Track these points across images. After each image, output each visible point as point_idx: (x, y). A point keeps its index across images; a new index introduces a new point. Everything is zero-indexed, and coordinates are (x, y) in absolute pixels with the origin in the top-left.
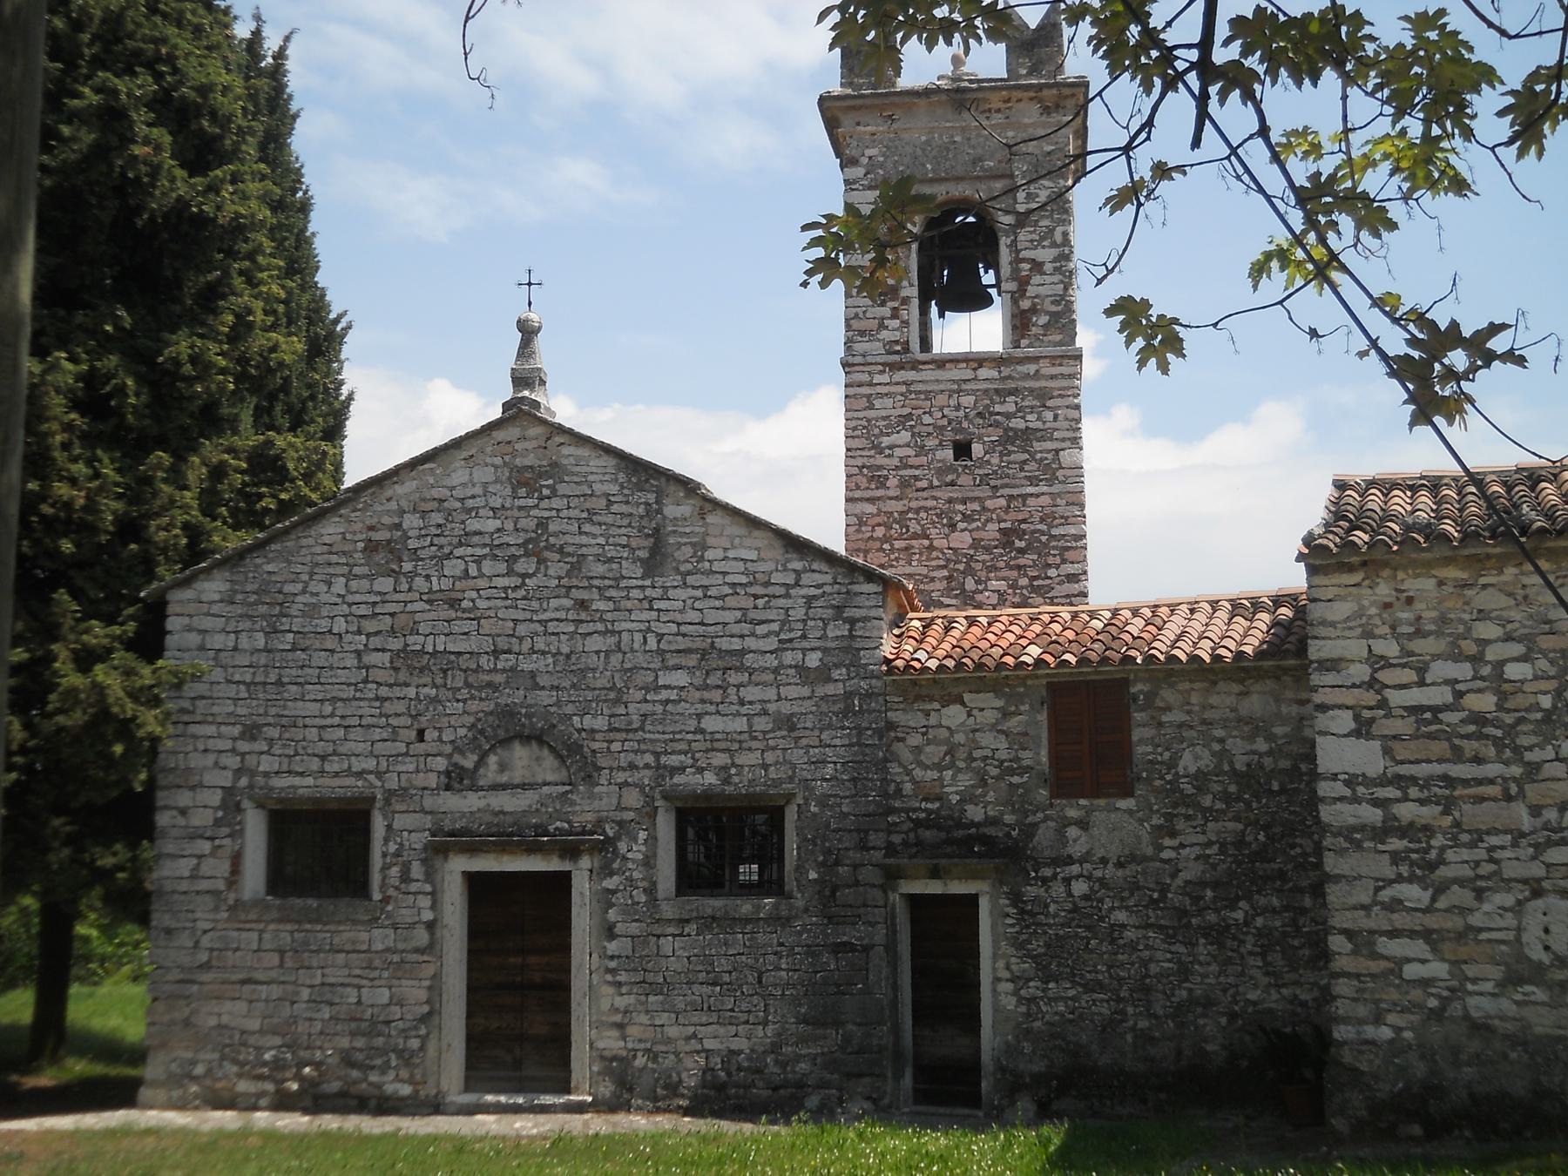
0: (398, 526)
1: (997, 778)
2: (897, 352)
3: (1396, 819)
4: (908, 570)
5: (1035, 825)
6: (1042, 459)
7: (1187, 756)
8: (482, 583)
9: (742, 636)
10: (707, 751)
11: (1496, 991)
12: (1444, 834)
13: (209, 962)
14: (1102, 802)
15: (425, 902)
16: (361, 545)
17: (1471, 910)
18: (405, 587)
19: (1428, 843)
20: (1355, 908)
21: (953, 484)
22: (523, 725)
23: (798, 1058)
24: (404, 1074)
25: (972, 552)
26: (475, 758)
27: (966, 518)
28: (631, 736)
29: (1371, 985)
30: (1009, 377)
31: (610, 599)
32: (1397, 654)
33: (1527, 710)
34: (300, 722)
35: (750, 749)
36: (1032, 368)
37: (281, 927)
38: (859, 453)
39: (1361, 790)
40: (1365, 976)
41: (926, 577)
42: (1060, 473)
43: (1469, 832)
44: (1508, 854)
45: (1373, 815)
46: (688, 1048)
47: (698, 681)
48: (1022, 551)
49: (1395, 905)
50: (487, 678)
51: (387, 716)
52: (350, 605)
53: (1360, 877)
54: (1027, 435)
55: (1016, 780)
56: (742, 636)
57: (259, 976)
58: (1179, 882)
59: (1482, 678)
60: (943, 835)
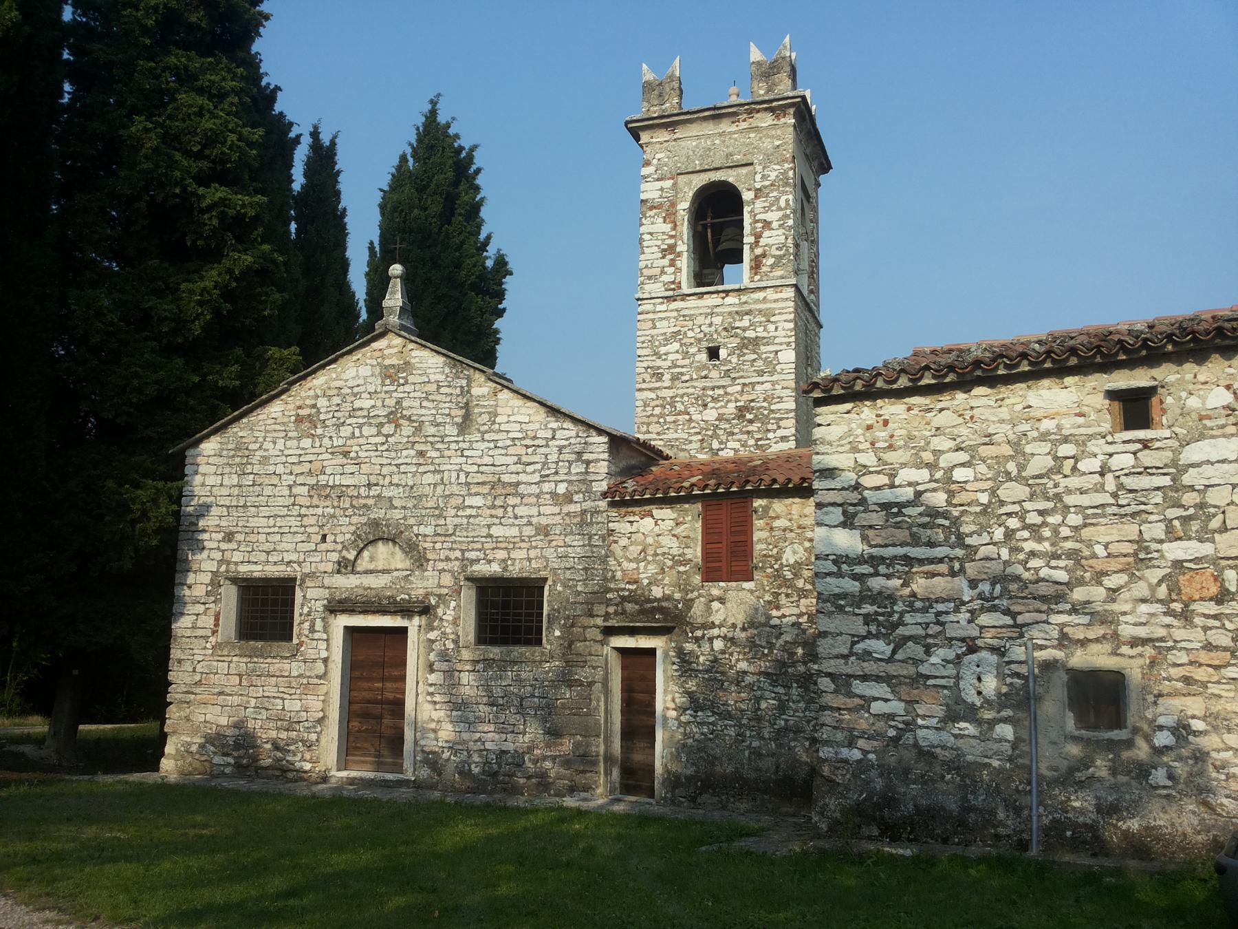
0: (314, 406)
1: (671, 568)
2: (674, 289)
3: (870, 590)
4: (675, 436)
5: (692, 600)
6: (766, 358)
7: (788, 550)
8: (362, 441)
9: (518, 473)
10: (493, 549)
11: (939, 726)
12: (904, 602)
13: (200, 681)
14: (734, 584)
15: (323, 645)
16: (293, 418)
17: (922, 662)
18: (317, 444)
19: (892, 608)
20: (837, 657)
21: (705, 377)
22: (384, 532)
23: (545, 758)
24: (307, 756)
25: (717, 423)
26: (355, 553)
27: (714, 399)
28: (447, 539)
29: (847, 717)
30: (745, 303)
31: (438, 450)
32: (875, 463)
33: (969, 505)
34: (255, 532)
35: (520, 548)
36: (760, 295)
37: (241, 660)
38: (646, 358)
39: (844, 567)
40: (844, 709)
41: (686, 440)
42: (778, 368)
43: (922, 600)
44: (952, 618)
45: (853, 586)
46: (475, 748)
47: (489, 503)
48: (751, 422)
49: (867, 655)
50: (362, 501)
51: (305, 527)
52: (286, 456)
53: (841, 634)
54: (756, 342)
55: (682, 569)
56: (518, 473)
57: (227, 690)
58: (781, 642)
59: (936, 481)
60: (637, 607)
